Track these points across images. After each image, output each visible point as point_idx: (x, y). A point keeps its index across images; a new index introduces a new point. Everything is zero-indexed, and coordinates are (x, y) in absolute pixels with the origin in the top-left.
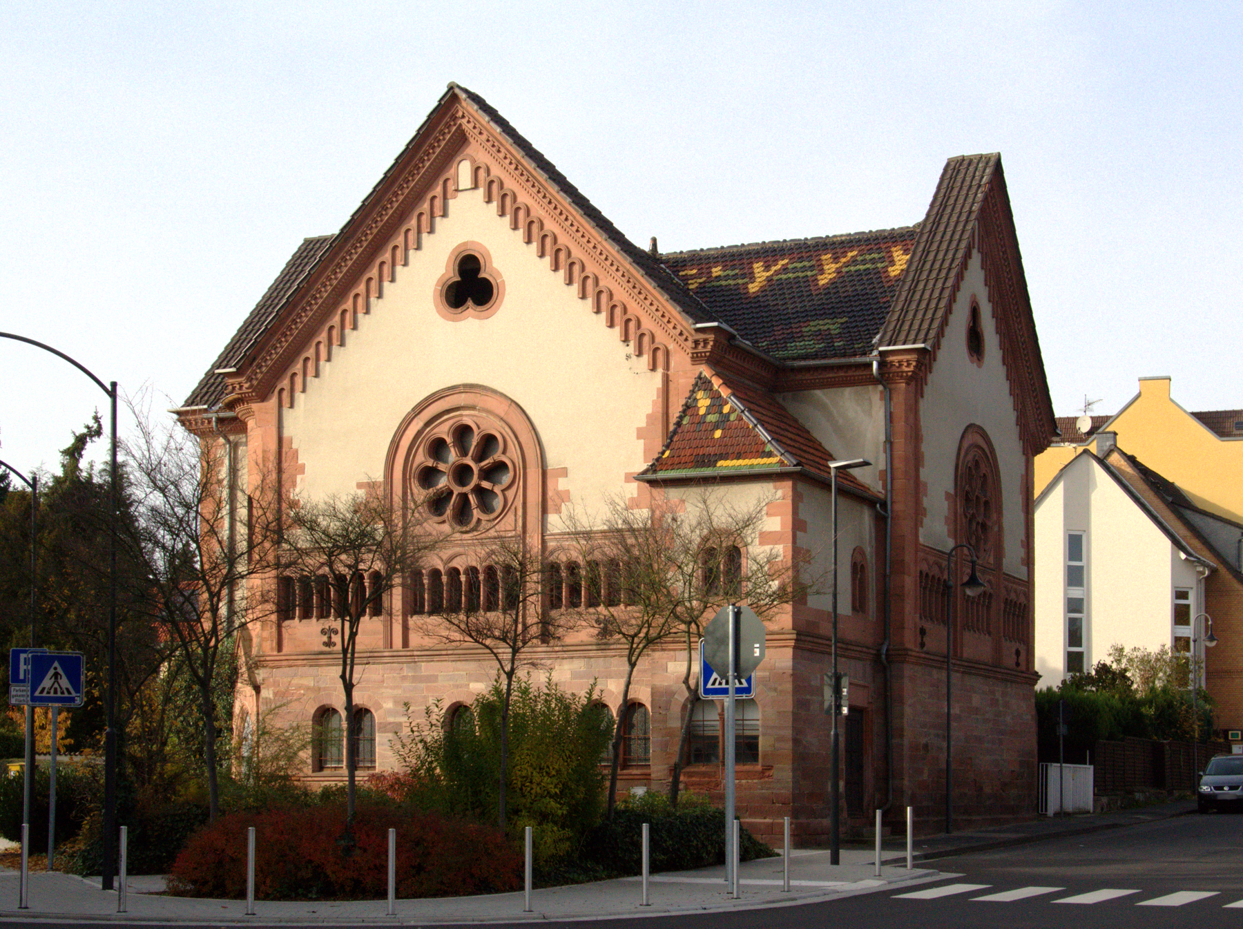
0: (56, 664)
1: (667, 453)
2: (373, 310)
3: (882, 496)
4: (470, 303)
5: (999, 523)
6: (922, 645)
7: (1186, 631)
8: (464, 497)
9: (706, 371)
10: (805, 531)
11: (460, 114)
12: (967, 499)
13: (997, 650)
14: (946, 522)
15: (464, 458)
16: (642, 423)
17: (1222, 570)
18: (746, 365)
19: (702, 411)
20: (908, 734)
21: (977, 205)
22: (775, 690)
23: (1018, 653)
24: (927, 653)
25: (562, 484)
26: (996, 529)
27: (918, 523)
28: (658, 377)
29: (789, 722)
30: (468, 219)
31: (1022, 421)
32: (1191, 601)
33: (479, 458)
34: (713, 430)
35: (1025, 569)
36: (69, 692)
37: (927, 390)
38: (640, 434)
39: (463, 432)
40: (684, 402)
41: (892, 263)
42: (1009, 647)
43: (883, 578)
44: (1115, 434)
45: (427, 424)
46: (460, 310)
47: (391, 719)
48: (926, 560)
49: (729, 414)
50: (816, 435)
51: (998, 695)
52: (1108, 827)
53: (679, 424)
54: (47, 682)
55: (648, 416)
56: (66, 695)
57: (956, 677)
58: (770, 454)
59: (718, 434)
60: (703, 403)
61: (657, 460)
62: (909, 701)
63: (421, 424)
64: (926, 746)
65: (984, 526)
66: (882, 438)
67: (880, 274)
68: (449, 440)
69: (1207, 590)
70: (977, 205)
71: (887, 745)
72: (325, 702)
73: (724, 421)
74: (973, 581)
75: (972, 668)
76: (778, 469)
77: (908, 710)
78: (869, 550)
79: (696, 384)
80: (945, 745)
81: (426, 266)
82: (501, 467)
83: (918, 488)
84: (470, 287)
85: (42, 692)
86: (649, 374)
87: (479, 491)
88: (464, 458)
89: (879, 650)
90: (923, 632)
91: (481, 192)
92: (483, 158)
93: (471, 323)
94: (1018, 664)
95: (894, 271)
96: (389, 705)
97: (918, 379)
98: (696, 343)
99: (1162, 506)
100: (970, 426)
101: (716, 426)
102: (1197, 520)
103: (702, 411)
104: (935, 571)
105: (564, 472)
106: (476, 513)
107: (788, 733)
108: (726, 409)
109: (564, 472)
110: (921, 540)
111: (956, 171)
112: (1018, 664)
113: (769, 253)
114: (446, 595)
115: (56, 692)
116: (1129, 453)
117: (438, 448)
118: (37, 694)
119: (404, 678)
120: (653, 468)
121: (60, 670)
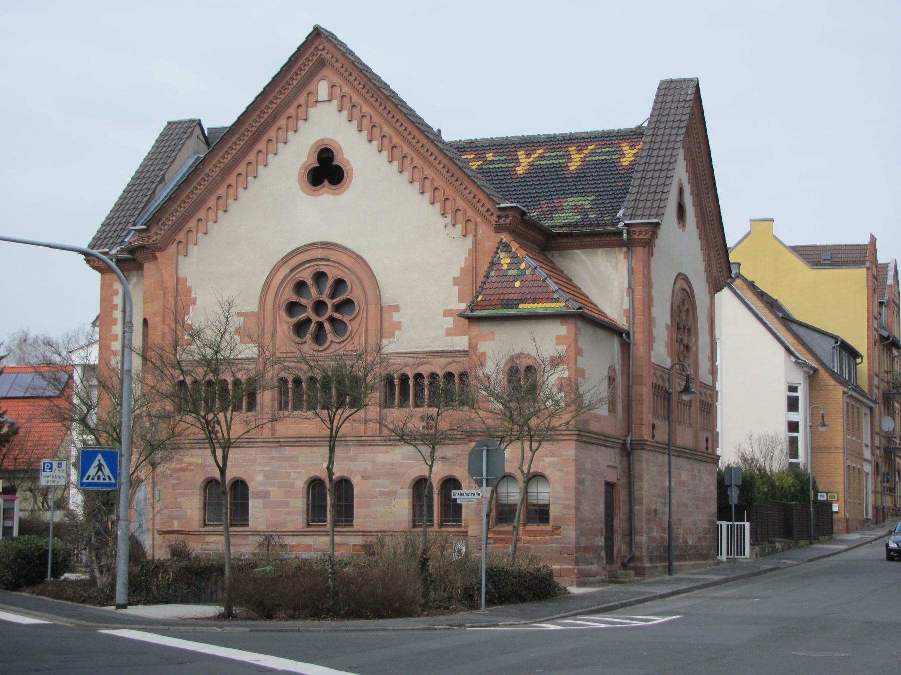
0: (99, 457)
1: (480, 298)
2: (250, 187)
3: (626, 329)
4: (326, 183)
5: (696, 345)
6: (653, 437)
7: (798, 417)
8: (320, 325)
9: (505, 238)
10: (581, 356)
11: (321, 48)
12: (678, 329)
13: (696, 439)
14: (666, 347)
15: (322, 296)
16: (457, 274)
17: (822, 371)
18: (529, 232)
19: (505, 267)
20: (645, 501)
21: (682, 113)
22: (562, 471)
23: (707, 440)
24: (657, 443)
25: (396, 317)
26: (694, 349)
27: (650, 348)
28: (469, 240)
29: (572, 495)
30: (326, 122)
31: (708, 270)
32: (800, 394)
33: (333, 296)
34: (514, 281)
35: (710, 377)
36: (110, 479)
37: (655, 250)
38: (455, 282)
39: (320, 277)
40: (490, 260)
41: (623, 155)
42: (703, 435)
43: (628, 388)
44: (739, 265)
45: (292, 271)
46: (319, 188)
47: (262, 489)
48: (655, 374)
49: (525, 269)
50: (577, 282)
51: (696, 472)
52: (771, 570)
53: (487, 276)
54: (92, 471)
55: (461, 269)
56: (107, 481)
57: (673, 458)
58: (557, 301)
59: (517, 284)
60: (505, 261)
61: (473, 302)
62: (646, 478)
63: (288, 271)
64: (655, 511)
65: (687, 347)
66: (626, 286)
67: (615, 164)
68: (310, 282)
69: (810, 386)
70: (682, 113)
71: (631, 511)
72: (209, 476)
73: (521, 275)
74: (686, 390)
75: (684, 453)
76: (564, 310)
77: (645, 485)
78: (618, 367)
79: (498, 248)
80: (667, 509)
81: (294, 154)
82: (349, 303)
83: (650, 322)
84: (326, 171)
85: (88, 479)
86: (462, 239)
87: (332, 320)
88: (322, 296)
89: (625, 441)
90: (654, 427)
91: (335, 103)
92: (336, 79)
93: (327, 199)
94: (707, 449)
95: (625, 162)
96: (260, 478)
97: (649, 244)
98: (499, 217)
99: (775, 321)
100: (680, 274)
101: (516, 278)
102: (801, 332)
103: (505, 267)
104: (660, 383)
105: (397, 309)
106: (330, 337)
107: (572, 503)
108: (522, 266)
109: (397, 309)
110: (653, 360)
111: (668, 89)
112: (707, 449)
113: (529, 144)
114: (297, 393)
115: (99, 478)
116: (750, 280)
117: (300, 287)
118: (84, 481)
119: (272, 458)
120: (473, 306)
121: (103, 462)
